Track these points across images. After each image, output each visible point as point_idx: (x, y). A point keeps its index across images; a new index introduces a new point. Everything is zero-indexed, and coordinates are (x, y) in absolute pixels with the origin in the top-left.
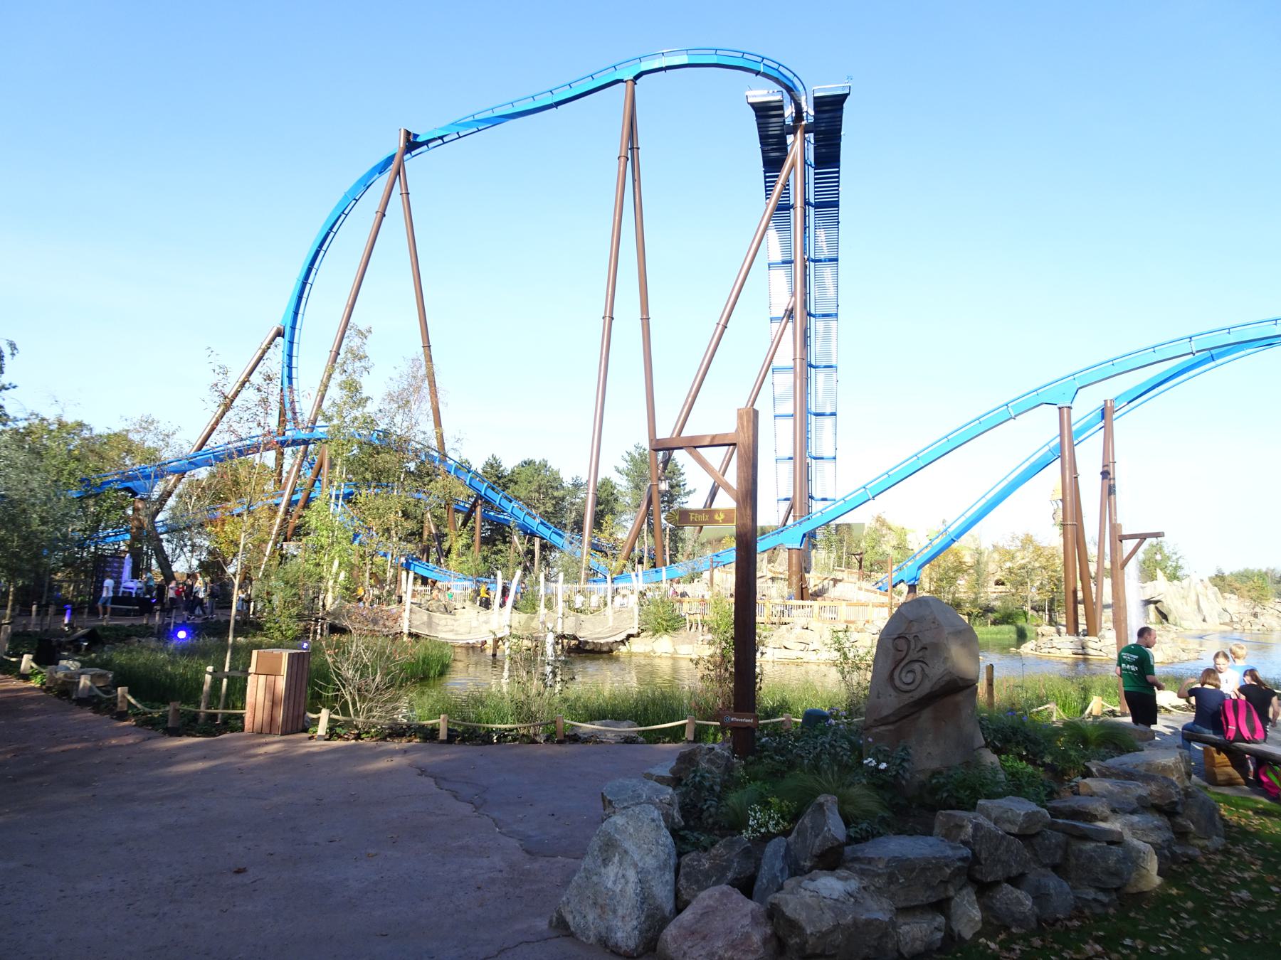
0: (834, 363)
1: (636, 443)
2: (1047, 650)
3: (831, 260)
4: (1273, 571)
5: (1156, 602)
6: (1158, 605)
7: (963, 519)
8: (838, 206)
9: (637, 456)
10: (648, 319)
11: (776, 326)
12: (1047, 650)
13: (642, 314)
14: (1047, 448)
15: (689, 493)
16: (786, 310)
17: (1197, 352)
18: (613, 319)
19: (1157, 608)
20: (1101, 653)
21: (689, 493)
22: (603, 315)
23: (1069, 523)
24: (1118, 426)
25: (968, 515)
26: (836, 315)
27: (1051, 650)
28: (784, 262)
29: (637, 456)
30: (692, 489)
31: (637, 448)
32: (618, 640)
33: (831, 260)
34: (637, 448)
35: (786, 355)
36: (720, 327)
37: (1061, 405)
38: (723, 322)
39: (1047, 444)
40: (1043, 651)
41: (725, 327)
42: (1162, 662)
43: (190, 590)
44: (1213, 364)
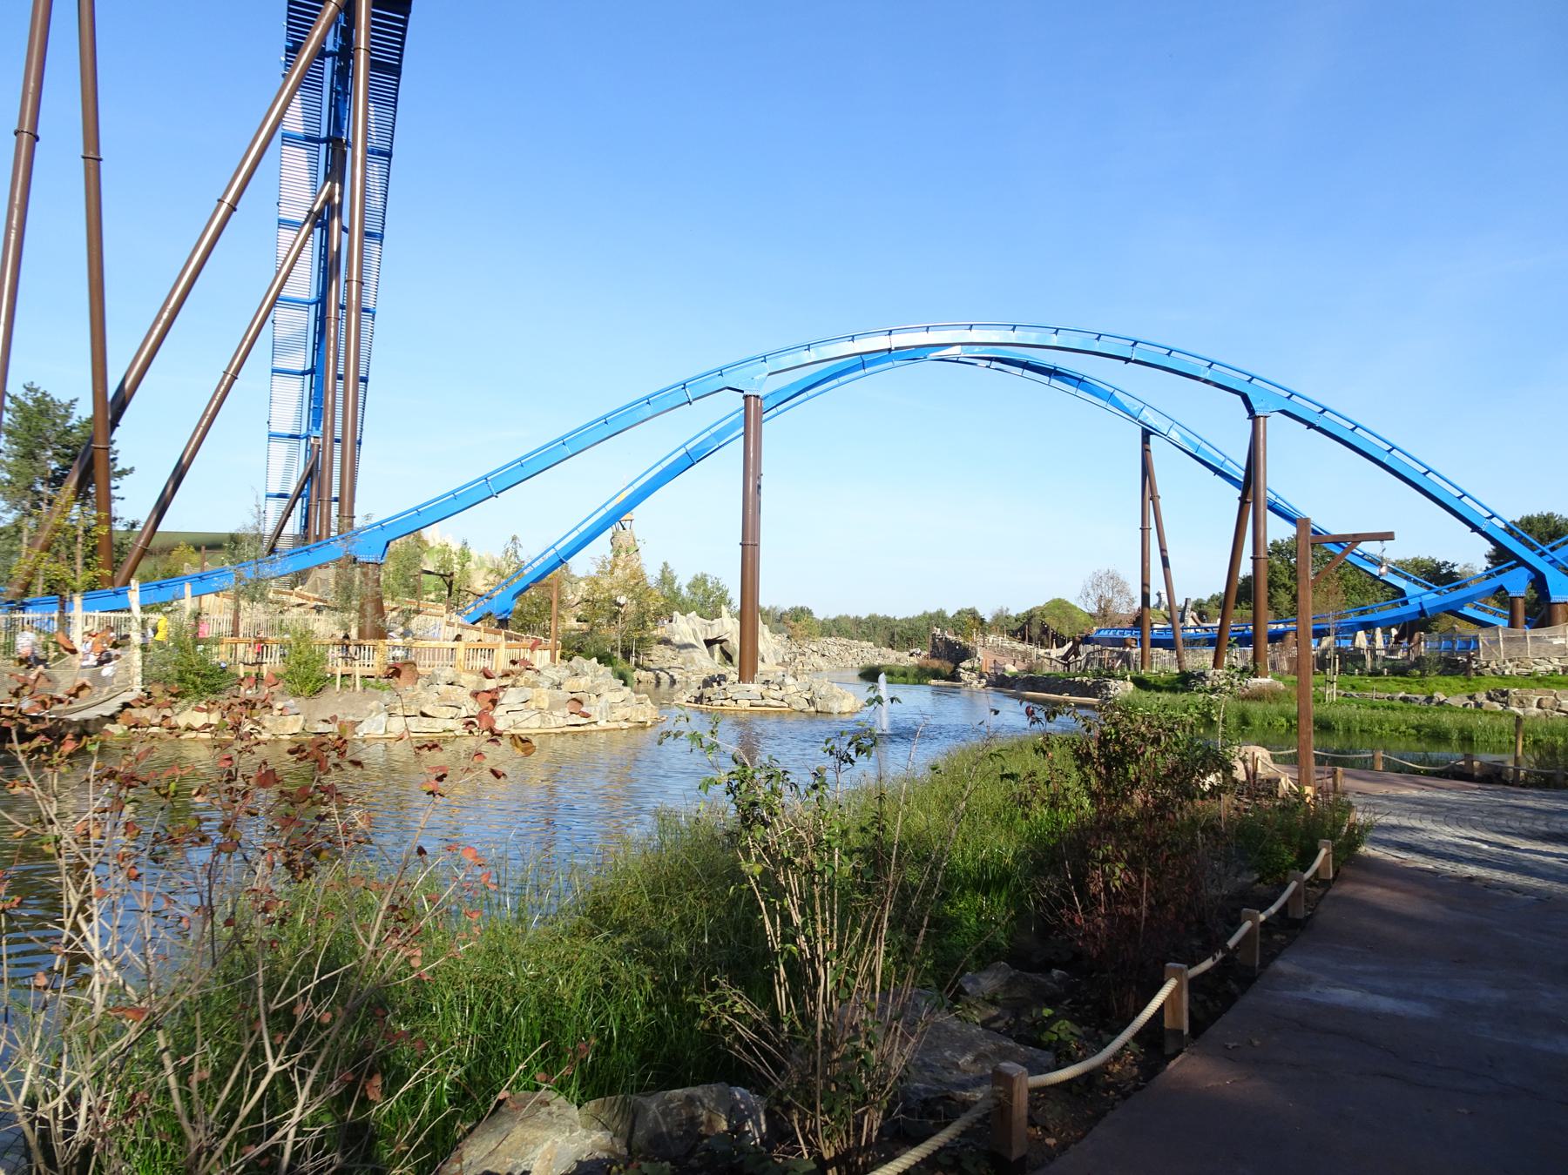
0: (371, 306)
1: (27, 381)
2: (720, 702)
3: (381, 153)
4: (775, 609)
5: (721, 642)
6: (724, 645)
7: (575, 534)
8: (398, 74)
9: (30, 403)
10: (100, 160)
11: (287, 236)
12: (720, 702)
13: (86, 148)
14: (683, 451)
15: (124, 472)
16: (310, 212)
17: (896, 349)
18: (37, 139)
19: (721, 648)
20: (783, 704)
21: (124, 472)
22: (16, 127)
23: (750, 542)
24: (771, 429)
25: (582, 529)
26: (382, 236)
27: (725, 702)
28: (308, 139)
29: (30, 403)
30: (128, 467)
31: (28, 389)
32: (107, 713)
33: (381, 153)
34: (28, 389)
35: (304, 283)
36: (224, 207)
37: (746, 393)
38: (229, 199)
39: (684, 446)
40: (715, 703)
41: (232, 208)
42: (850, 712)
43: (1229, 817)
44: (862, 372)
